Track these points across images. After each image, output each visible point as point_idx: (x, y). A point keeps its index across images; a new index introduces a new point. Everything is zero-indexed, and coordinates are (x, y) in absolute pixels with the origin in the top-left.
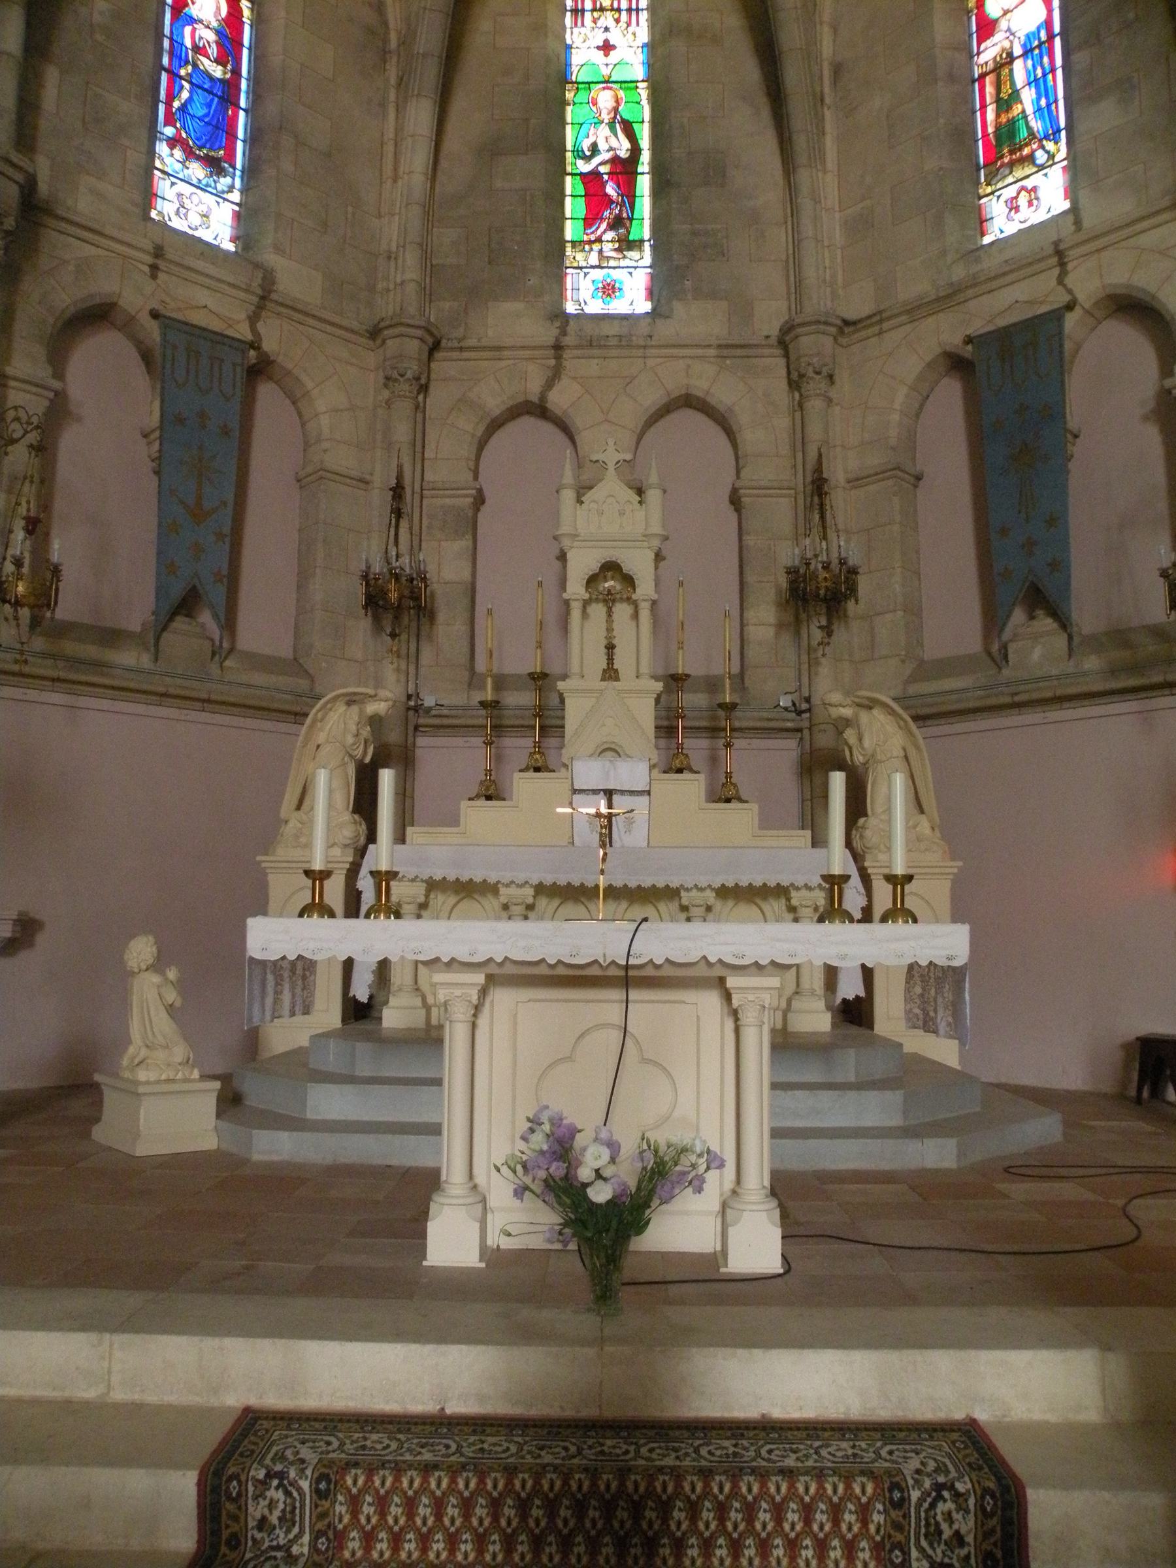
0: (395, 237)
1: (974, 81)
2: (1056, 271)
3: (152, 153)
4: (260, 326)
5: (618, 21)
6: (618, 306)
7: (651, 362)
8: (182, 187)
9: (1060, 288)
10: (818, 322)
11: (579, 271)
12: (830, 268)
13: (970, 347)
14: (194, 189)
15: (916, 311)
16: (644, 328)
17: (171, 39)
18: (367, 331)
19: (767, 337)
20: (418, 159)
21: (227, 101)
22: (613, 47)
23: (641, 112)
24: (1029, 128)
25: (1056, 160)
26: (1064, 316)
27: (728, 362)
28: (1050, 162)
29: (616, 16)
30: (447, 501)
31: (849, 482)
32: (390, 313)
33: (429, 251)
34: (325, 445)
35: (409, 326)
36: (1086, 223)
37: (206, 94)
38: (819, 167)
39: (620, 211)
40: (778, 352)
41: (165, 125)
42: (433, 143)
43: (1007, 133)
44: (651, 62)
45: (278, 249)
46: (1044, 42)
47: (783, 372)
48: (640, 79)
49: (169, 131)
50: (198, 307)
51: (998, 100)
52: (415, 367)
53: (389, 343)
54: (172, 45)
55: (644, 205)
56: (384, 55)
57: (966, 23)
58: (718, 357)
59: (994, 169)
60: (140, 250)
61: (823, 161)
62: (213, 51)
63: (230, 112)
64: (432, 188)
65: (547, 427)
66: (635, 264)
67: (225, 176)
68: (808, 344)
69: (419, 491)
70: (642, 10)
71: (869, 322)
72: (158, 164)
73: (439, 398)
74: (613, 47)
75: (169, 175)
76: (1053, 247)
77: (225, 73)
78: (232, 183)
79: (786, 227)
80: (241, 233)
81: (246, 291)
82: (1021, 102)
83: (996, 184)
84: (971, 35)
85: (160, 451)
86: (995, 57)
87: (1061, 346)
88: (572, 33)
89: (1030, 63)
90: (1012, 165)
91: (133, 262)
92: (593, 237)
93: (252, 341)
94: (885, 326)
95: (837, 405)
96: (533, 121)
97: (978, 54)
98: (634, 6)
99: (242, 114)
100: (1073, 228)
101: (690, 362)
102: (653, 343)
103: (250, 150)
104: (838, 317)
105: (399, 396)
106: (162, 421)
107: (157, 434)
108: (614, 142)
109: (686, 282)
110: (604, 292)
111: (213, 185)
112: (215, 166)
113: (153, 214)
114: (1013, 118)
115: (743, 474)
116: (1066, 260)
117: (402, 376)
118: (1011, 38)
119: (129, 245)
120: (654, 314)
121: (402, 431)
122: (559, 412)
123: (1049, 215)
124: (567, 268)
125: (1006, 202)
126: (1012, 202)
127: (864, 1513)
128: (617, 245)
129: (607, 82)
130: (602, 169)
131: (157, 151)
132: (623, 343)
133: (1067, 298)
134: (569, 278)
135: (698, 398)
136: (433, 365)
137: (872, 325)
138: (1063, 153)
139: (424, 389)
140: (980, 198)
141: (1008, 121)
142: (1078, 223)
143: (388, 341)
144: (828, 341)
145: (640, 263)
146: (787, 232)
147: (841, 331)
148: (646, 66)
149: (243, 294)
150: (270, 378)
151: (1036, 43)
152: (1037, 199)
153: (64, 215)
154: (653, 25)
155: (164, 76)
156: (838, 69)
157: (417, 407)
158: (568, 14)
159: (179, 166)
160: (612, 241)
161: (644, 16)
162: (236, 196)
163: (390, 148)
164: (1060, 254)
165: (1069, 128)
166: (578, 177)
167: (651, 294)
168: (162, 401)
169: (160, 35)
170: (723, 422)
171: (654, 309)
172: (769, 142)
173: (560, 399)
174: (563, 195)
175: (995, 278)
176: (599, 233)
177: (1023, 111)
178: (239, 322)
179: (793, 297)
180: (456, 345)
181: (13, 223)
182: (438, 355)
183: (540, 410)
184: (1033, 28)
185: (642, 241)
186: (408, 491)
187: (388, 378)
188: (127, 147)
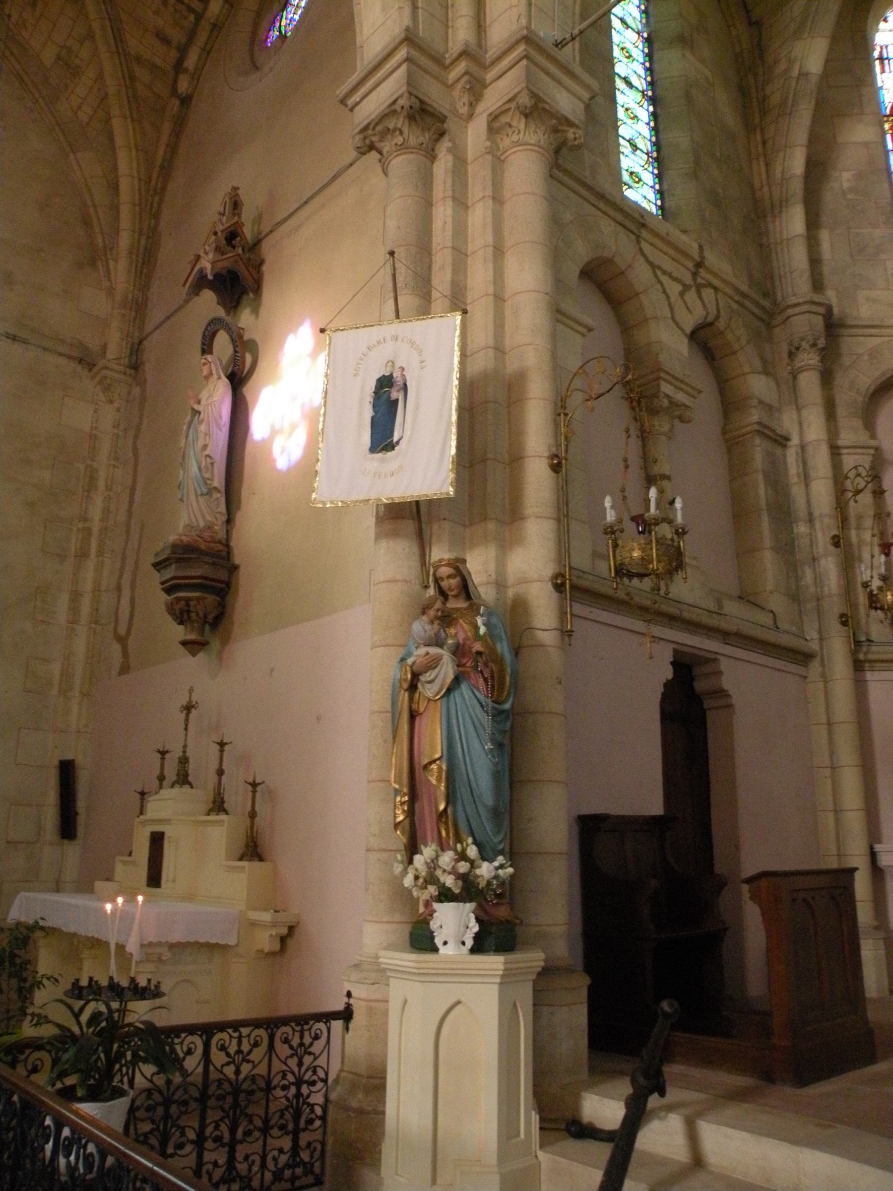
30: (192, 573)
58: (540, 926)
127: (120, 1070)
153: (853, 323)
181: (824, 342)
188: (886, 260)
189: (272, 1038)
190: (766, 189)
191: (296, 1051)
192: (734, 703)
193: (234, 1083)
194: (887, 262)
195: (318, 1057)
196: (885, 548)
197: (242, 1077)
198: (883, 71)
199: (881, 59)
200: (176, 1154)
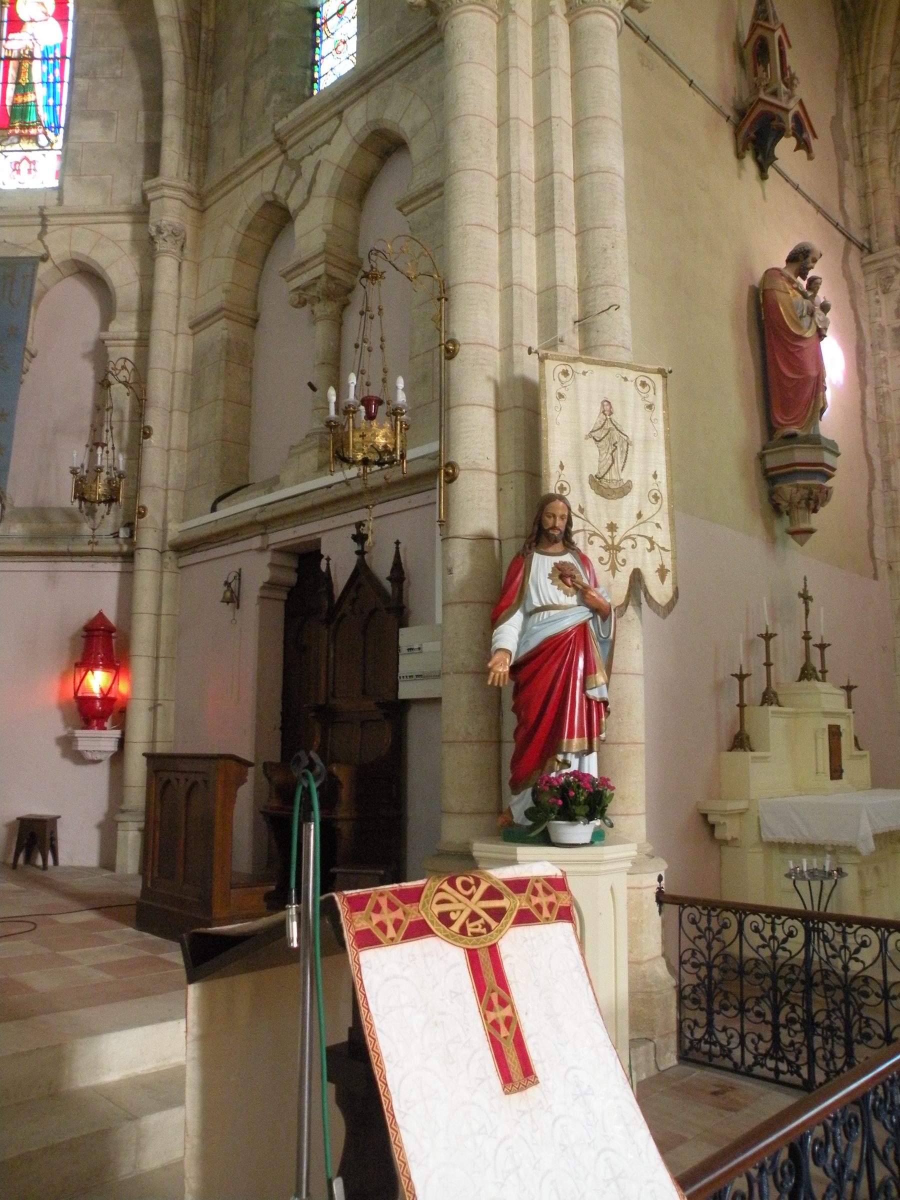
24: (37, 115)
25: (54, 147)
26: (38, 264)
28: (49, 148)
46: (58, 59)
51: (17, 83)
76: (39, 209)
87: (32, 285)
90: (20, 137)
97: (7, 40)
100: (56, 202)
114: (27, 102)
133: (42, 251)
141: (23, 103)
142: (60, 199)
164: (44, 218)
165: (67, 128)
189: (741, 924)
191: (705, 934)
193: (843, 979)
195: (867, 967)
196: (893, 64)
197: (713, 953)
200: (862, 1042)
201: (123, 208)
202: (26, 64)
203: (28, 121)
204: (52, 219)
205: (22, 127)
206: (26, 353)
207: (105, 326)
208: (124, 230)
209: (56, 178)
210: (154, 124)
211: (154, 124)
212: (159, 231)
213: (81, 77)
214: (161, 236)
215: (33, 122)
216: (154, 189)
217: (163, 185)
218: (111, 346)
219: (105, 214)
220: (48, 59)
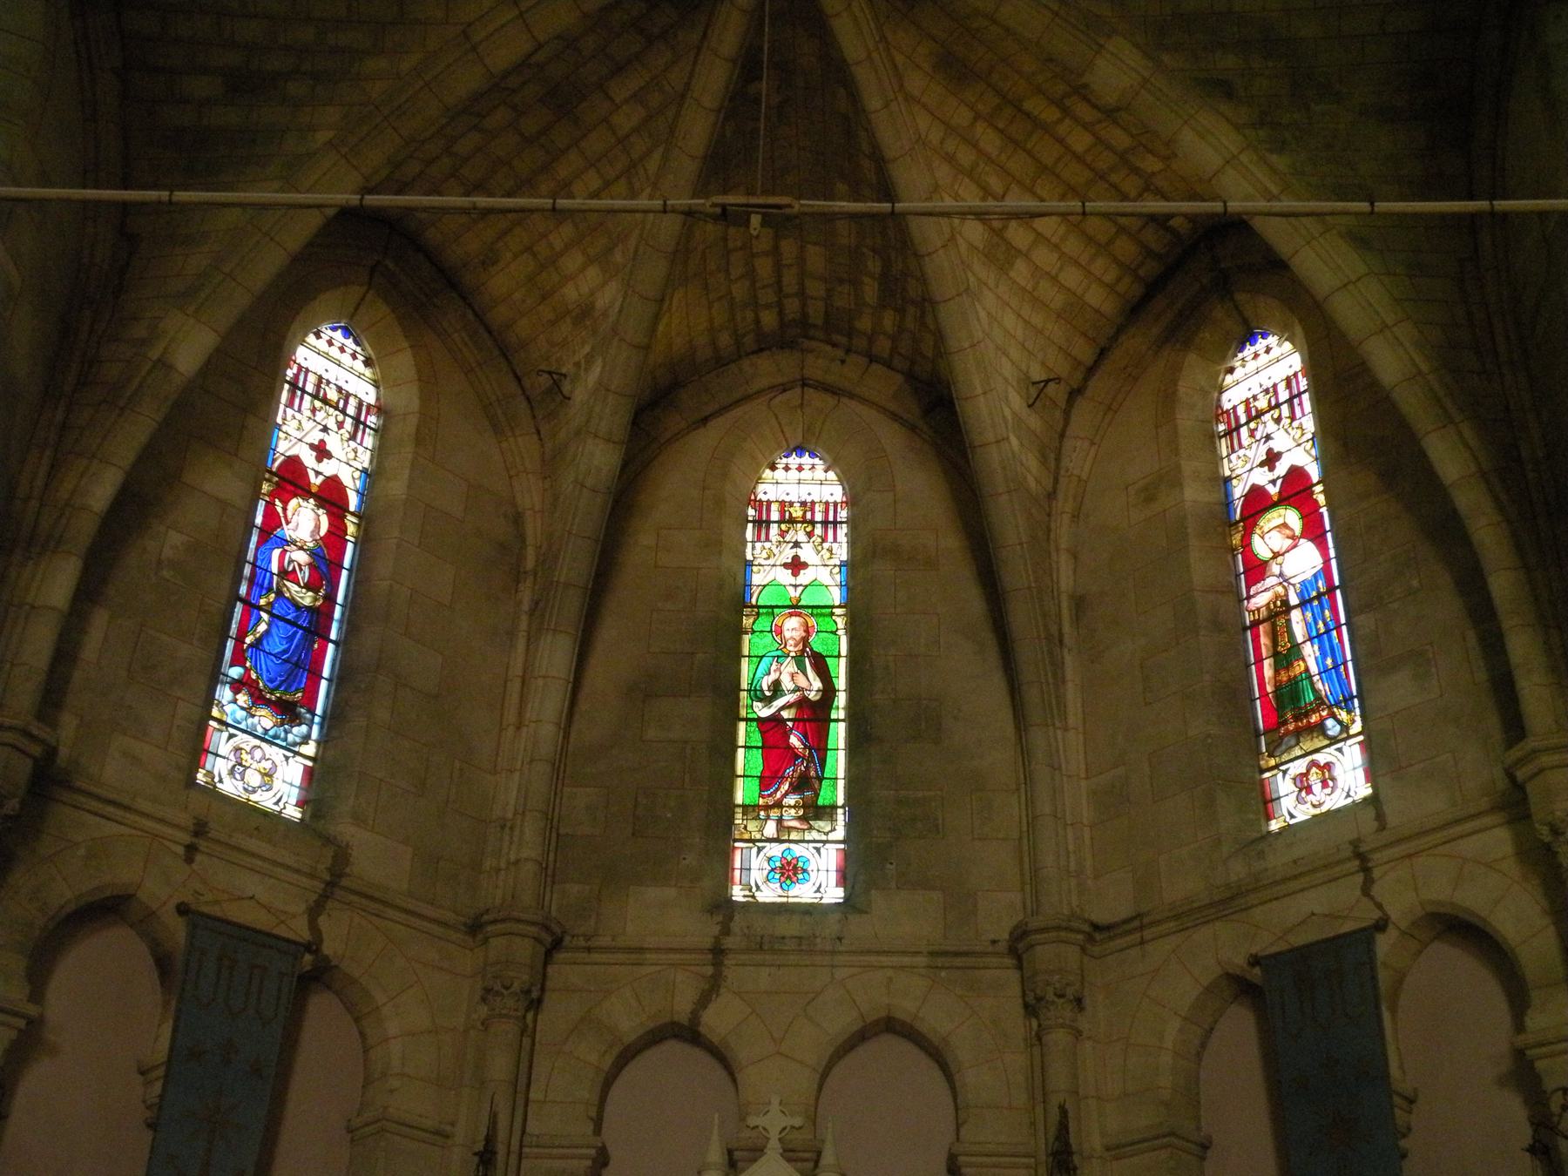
0: (512, 802)
1: (1245, 629)
2: (1360, 878)
3: (210, 700)
4: (323, 921)
5: (810, 535)
6: (802, 893)
7: (840, 973)
8: (241, 738)
9: (1365, 900)
10: (1058, 928)
11: (751, 845)
12: (1075, 852)
13: (1257, 970)
14: (257, 742)
15: (1189, 916)
16: (832, 926)
17: (254, 565)
18: (465, 924)
19: (994, 942)
20: (548, 704)
21: (315, 633)
22: (805, 565)
23: (836, 644)
24: (1315, 691)
25: (1352, 732)
26: (1373, 938)
27: (943, 974)
28: (1345, 735)
29: (809, 529)
30: (558, 1164)
31: (1108, 1149)
32: (498, 901)
33: (555, 820)
34: (395, 1083)
35: (519, 921)
36: (1392, 820)
37: (289, 627)
38: (1058, 724)
39: (807, 768)
40: (1009, 961)
41: (231, 666)
42: (570, 685)
43: (1289, 695)
44: (851, 585)
45: (358, 819)
46: (1323, 594)
47: (1016, 990)
48: (837, 603)
49: (236, 672)
50: (240, 898)
51: (1276, 655)
52: (525, 977)
53: (493, 942)
54: (253, 573)
55: (837, 762)
56: (517, 575)
57: (1231, 563)
58: (929, 967)
59: (1277, 736)
60: (177, 826)
61: (1064, 716)
62: (304, 576)
63: (316, 646)
64: (567, 736)
65: (698, 1053)
66: (824, 838)
67: (299, 725)
68: (1044, 954)
69: (517, 1147)
70: (841, 523)
71: (1127, 927)
72: (215, 712)
73: (556, 1015)
74: (805, 565)
75: (228, 725)
76: (1351, 848)
77: (316, 600)
78: (308, 736)
79: (1019, 797)
80: (312, 796)
81: (312, 876)
82: (1304, 660)
83: (1280, 756)
84: (1238, 576)
85: (161, 1097)
86: (1269, 604)
87: (1374, 978)
88: (753, 548)
89: (1309, 615)
90: (1298, 734)
91: (167, 843)
92: (770, 801)
93: (309, 942)
94: (1147, 934)
95: (1089, 1038)
96: (700, 656)
97: (1249, 598)
98: (831, 518)
99: (331, 647)
100: (1376, 824)
101: (890, 973)
102: (842, 948)
103: (337, 691)
104: (1086, 921)
105: (501, 1016)
106: (170, 1057)
107: (161, 1072)
108: (802, 681)
109: (889, 866)
110: (783, 874)
111: (283, 735)
112: (288, 712)
113: (201, 777)
114: (1295, 677)
115: (963, 1132)
116: (1370, 865)
117: (507, 988)
118: (1285, 584)
119: (161, 821)
120: (848, 904)
121: (500, 1066)
122: (715, 1040)
123: (1349, 800)
124: (736, 840)
125: (1294, 779)
126: (1302, 781)
128: (801, 812)
129: (795, 608)
130: (785, 714)
131: (217, 697)
132: (804, 947)
133: (1376, 914)
134: (738, 855)
135: (903, 1023)
136: (550, 970)
137: (1130, 932)
138: (1357, 727)
139: (536, 1005)
140: (1263, 771)
141: (1290, 679)
142: (1380, 817)
143: (491, 940)
144: (1072, 955)
145: (832, 837)
146: (1019, 803)
147: (1090, 939)
148: (844, 589)
149: (304, 880)
150: (329, 987)
151: (1314, 594)
152: (1333, 779)
153: (84, 786)
154: (852, 544)
155: (239, 607)
156: (1080, 603)
157: (523, 1032)
158: (750, 526)
159: (241, 714)
160: (794, 807)
161: (843, 531)
162: (310, 749)
163: (515, 686)
164: (1362, 857)
165: (1360, 696)
166: (755, 724)
167: (844, 878)
168: (175, 1030)
169: (241, 560)
170: (937, 1054)
171: (847, 899)
172: (997, 684)
173: (718, 1020)
174: (734, 747)
175: (1285, 880)
176: (779, 795)
177: (1307, 670)
178: (294, 916)
179: (1028, 888)
180: (582, 943)
181: (17, 806)
182: (560, 956)
183: (690, 1033)
184: (1308, 575)
185: (834, 807)
186: (501, 1157)
187: (488, 990)
188: (179, 698)
190: (34, 504)
192: (180, 919)
194: (181, 703)
198: (290, 404)
199: (294, 385)
201: (1484, 803)
202: (1281, 621)
203: (1303, 704)
204: (1376, 856)
205: (1297, 718)
206: (1397, 1100)
207: (1519, 1027)
208: (1498, 840)
209: (1367, 782)
210: (1493, 644)
211: (1493, 644)
212: (1556, 832)
213: (1362, 612)
214: (1562, 839)
215: (1311, 704)
216: (1521, 761)
217: (1534, 751)
218: (1540, 1058)
219: (1457, 822)
220: (1311, 601)
